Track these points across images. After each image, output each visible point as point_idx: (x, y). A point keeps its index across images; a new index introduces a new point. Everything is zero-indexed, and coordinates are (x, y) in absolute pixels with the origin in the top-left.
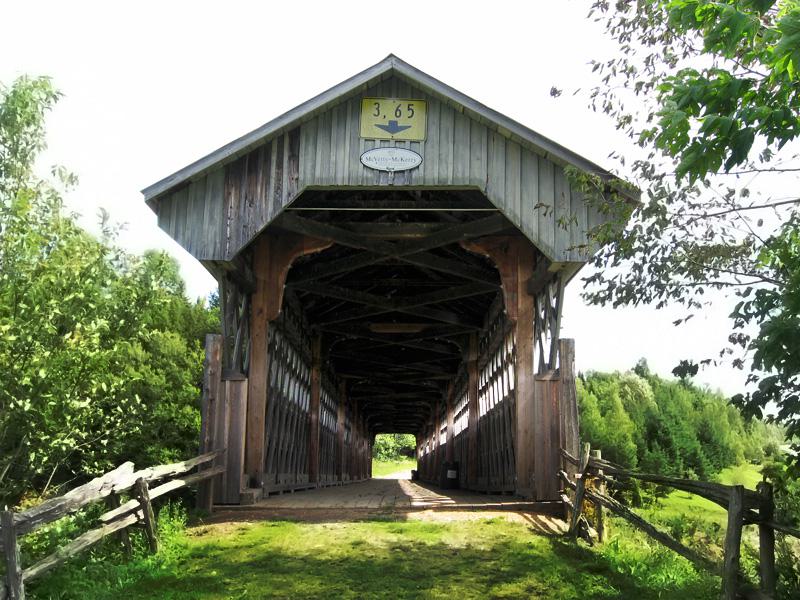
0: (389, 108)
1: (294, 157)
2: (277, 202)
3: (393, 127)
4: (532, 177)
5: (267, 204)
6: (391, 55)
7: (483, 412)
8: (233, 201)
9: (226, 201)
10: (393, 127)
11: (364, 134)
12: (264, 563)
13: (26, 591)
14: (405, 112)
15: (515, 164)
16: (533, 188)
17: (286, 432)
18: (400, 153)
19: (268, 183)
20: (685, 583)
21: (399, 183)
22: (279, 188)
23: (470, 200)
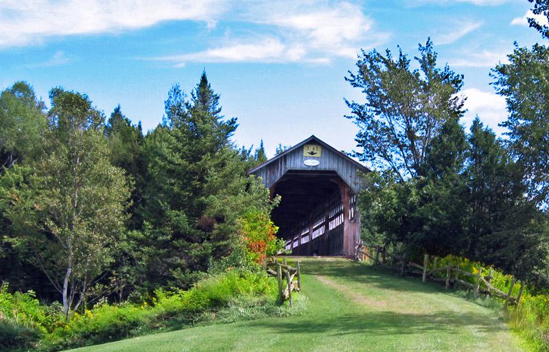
0: (311, 148)
1: (285, 162)
2: (281, 174)
3: (312, 153)
4: (350, 169)
5: (278, 176)
6: (313, 141)
7: (331, 228)
8: (269, 173)
9: (267, 173)
10: (312, 153)
11: (304, 155)
12: (370, 280)
13: (422, 275)
14: (316, 149)
15: (345, 166)
16: (350, 171)
17: (479, 328)
18: (314, 161)
19: (278, 169)
20: (166, 311)
21: (314, 169)
22: (281, 170)
23: (333, 174)
